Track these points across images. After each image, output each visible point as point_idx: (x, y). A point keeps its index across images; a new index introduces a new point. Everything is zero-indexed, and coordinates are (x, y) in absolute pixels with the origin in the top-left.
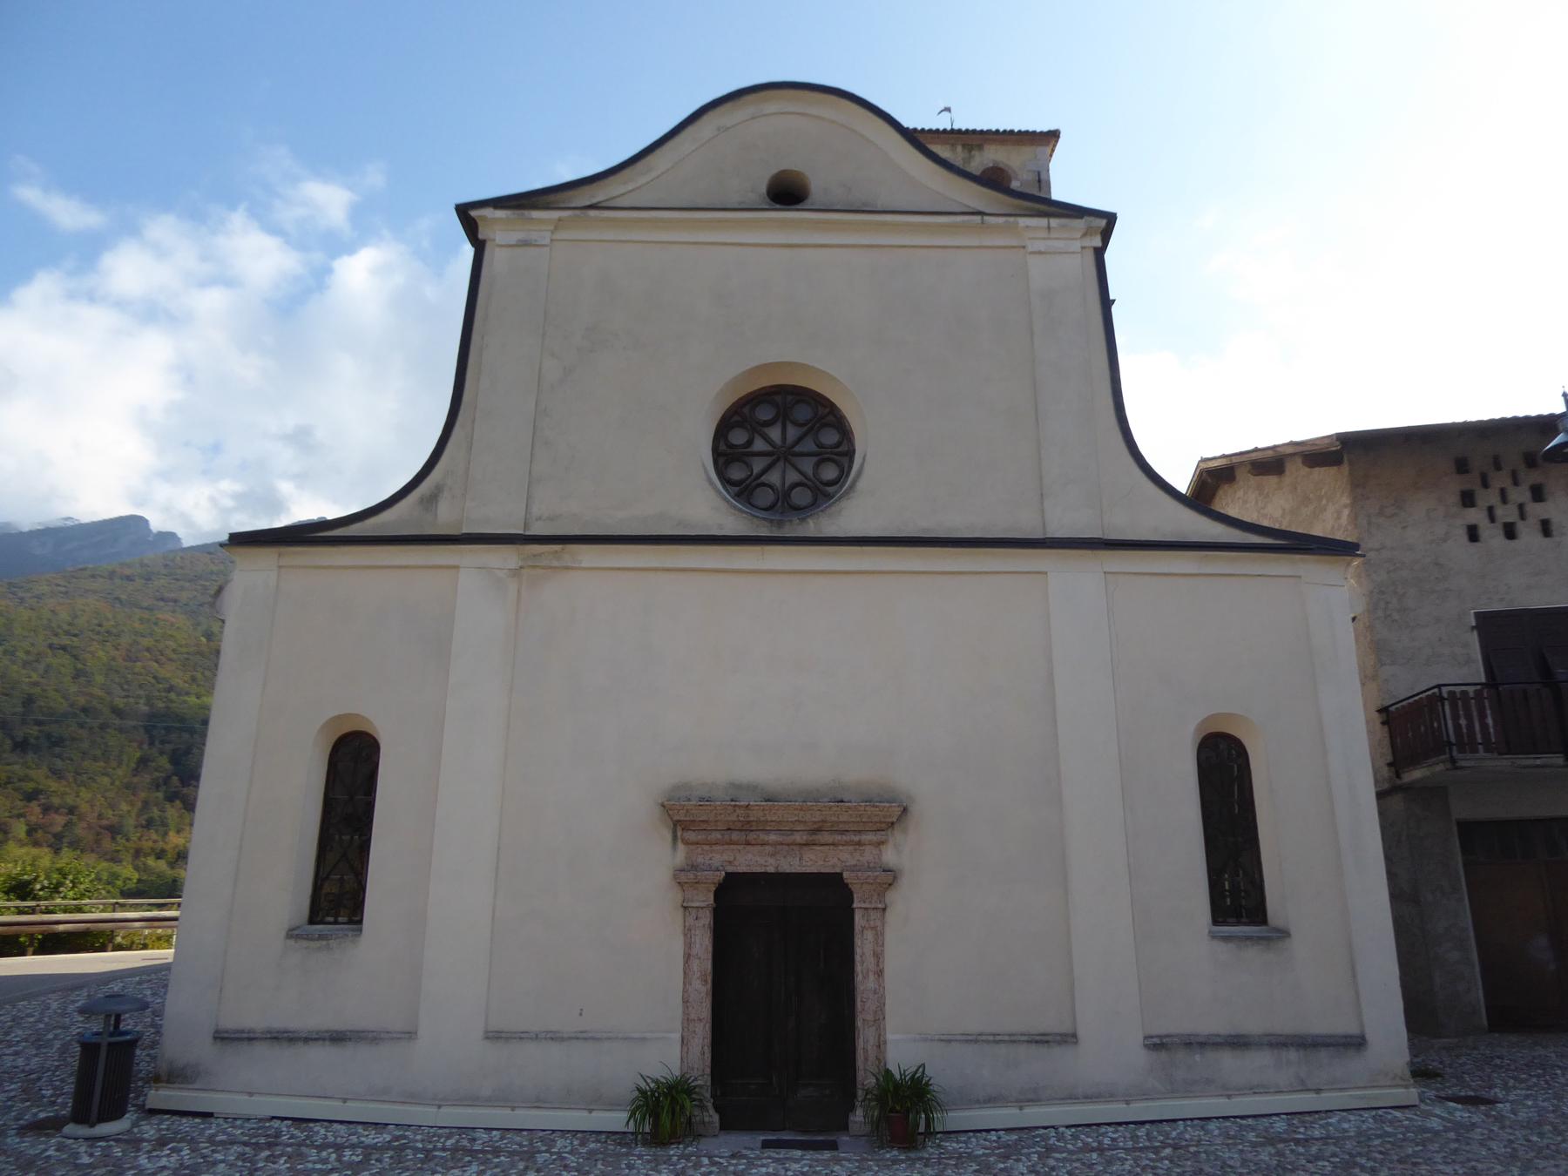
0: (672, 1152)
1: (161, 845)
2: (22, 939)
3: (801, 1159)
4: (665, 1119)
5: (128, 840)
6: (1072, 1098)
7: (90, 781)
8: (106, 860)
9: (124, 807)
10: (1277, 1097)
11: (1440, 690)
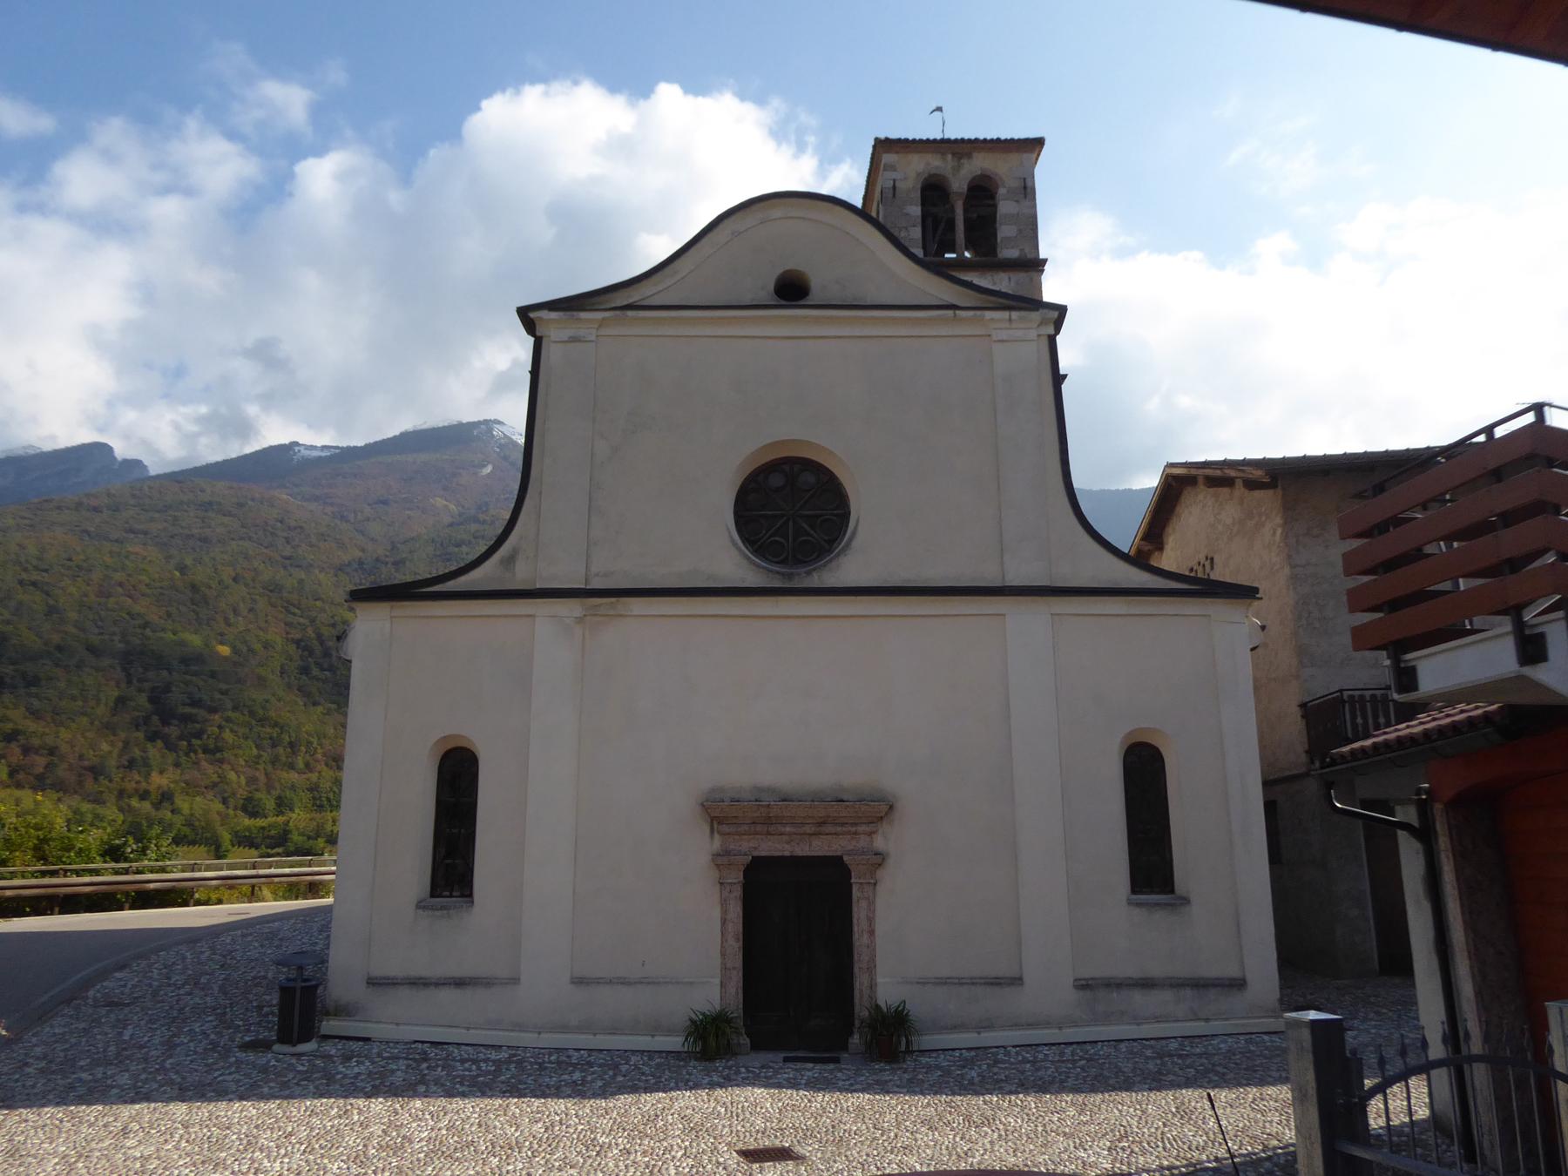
0: (718, 1065)
1: (144, 785)
2: (119, 896)
3: (813, 1069)
4: (712, 1042)
5: (111, 781)
6: (1016, 1025)
7: (69, 721)
8: (89, 801)
9: (105, 747)
10: (1175, 1025)
11: (1342, 695)
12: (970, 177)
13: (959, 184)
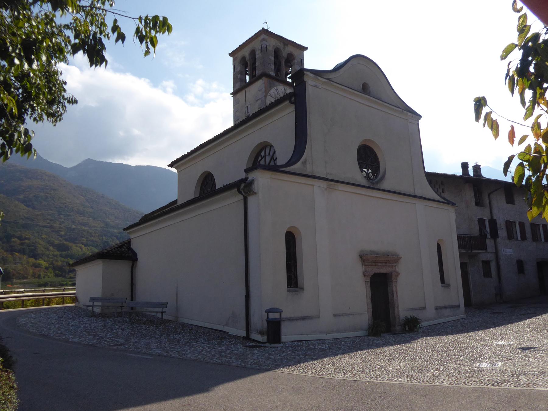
13: (284, 54)
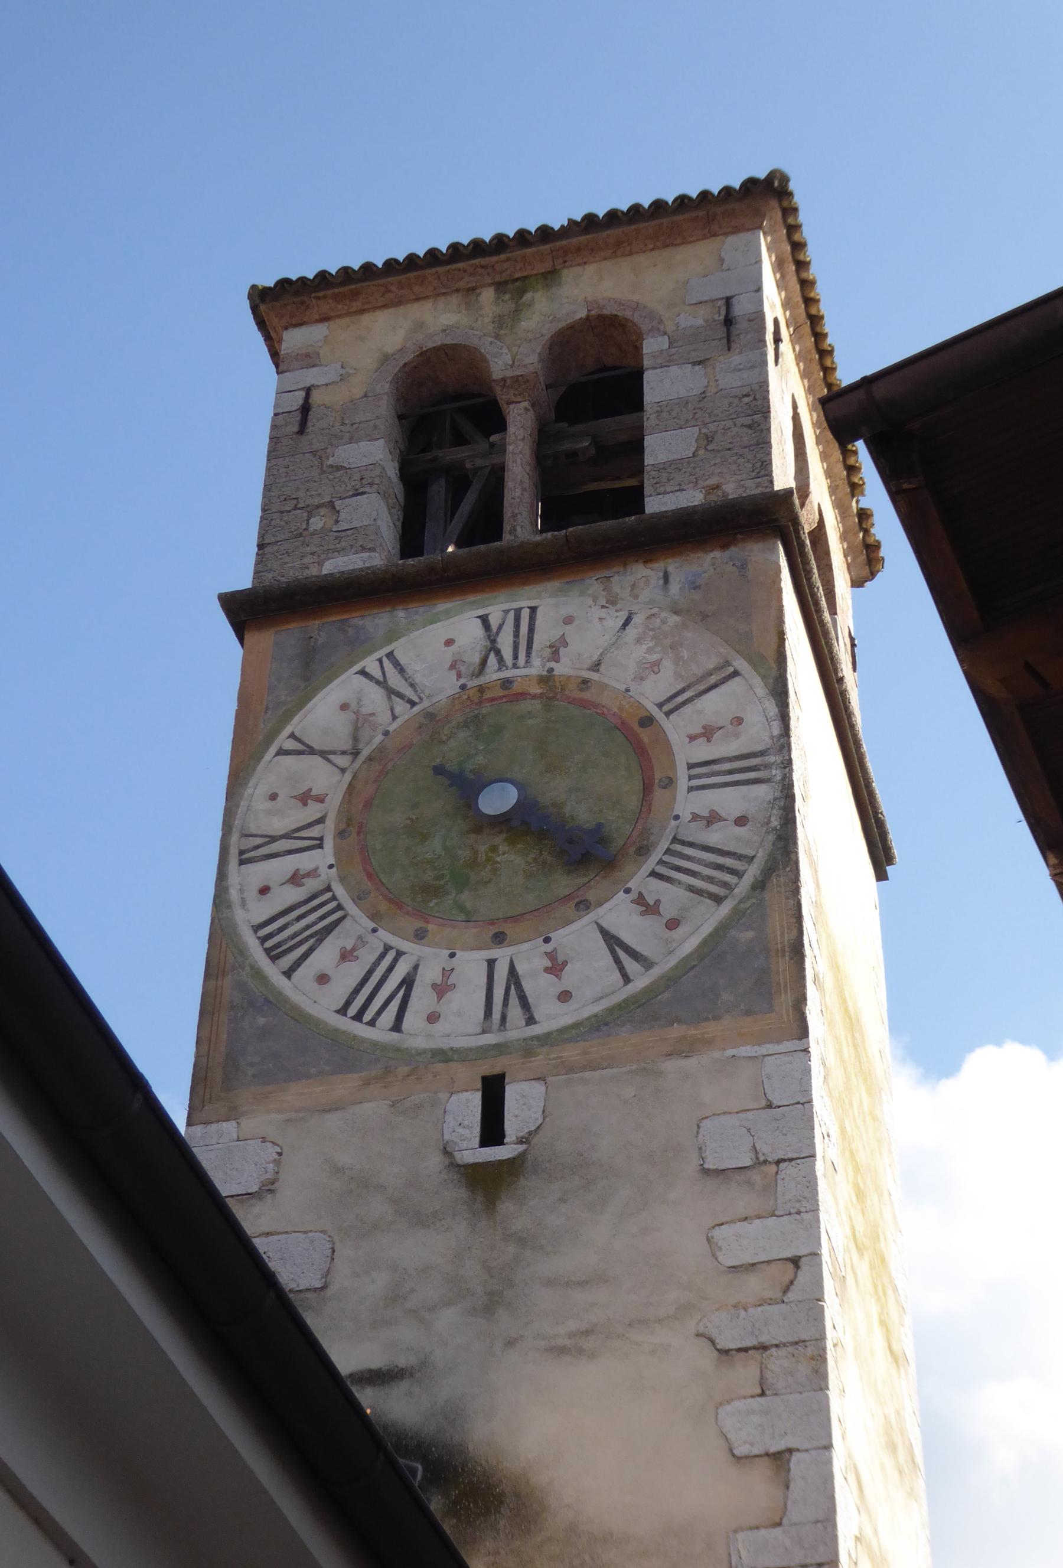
12: (550, 330)
